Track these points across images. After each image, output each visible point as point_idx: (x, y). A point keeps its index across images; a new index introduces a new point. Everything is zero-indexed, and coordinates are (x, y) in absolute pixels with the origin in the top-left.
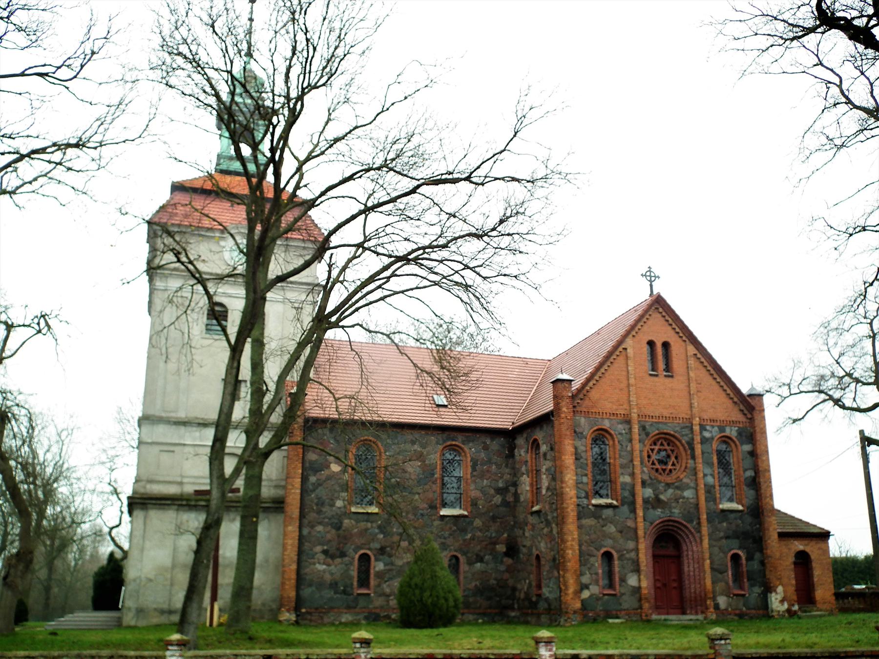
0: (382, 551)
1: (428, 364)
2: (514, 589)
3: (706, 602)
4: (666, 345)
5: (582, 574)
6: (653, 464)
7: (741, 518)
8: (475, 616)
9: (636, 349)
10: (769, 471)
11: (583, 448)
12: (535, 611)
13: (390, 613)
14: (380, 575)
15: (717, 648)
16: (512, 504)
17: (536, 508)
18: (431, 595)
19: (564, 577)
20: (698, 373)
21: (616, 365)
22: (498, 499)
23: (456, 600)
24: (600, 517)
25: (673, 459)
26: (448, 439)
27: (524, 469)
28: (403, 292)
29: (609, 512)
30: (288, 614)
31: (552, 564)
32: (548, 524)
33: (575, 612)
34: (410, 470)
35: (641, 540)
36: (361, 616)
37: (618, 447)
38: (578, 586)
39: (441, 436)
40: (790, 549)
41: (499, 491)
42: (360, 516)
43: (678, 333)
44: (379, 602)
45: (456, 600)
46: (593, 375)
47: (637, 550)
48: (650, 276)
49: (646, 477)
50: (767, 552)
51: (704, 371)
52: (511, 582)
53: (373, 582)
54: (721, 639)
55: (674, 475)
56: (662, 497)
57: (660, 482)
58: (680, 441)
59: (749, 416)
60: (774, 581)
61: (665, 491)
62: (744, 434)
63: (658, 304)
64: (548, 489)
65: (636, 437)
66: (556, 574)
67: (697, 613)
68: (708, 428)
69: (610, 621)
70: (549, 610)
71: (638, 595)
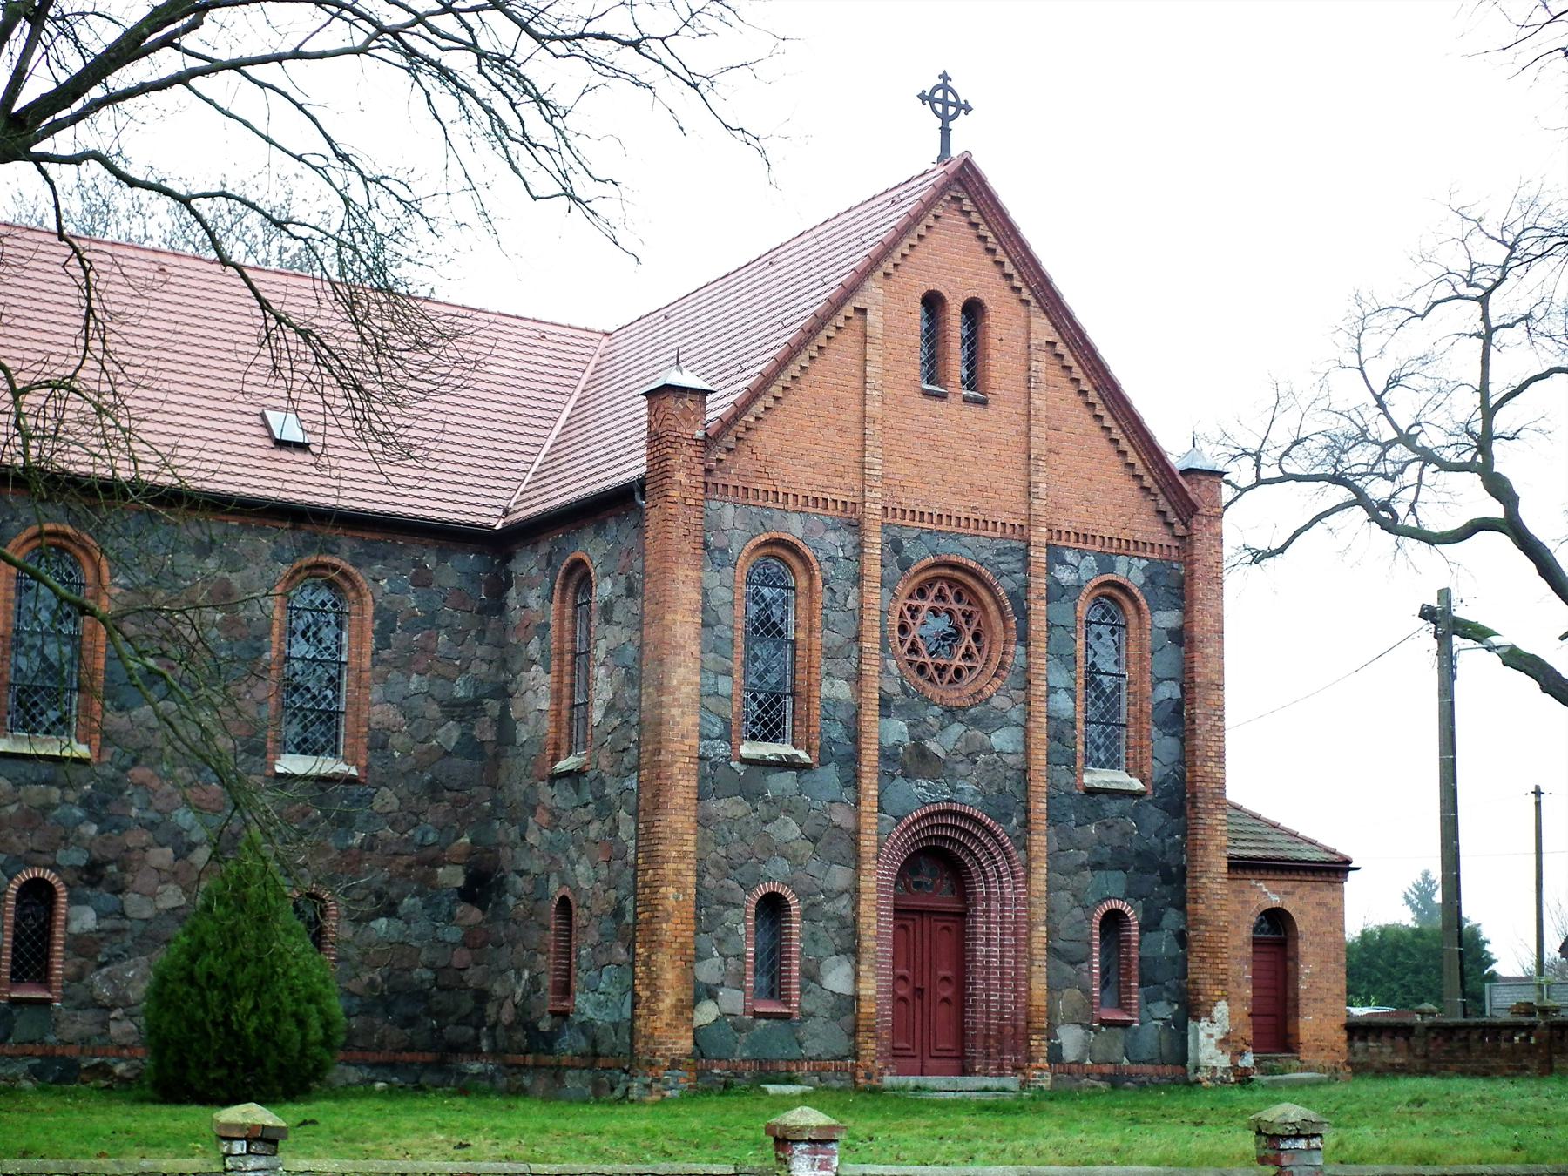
0: (92, 874)
1: (300, 300)
2: (482, 996)
3: (1028, 1040)
4: (973, 310)
5: (699, 957)
6: (913, 650)
7: (1136, 814)
8: (366, 1073)
9: (892, 315)
10: (1220, 687)
11: (725, 595)
12: (550, 1060)
13: (110, 1061)
14: (81, 945)
15: (1285, 1162)
16: (489, 750)
17: (562, 765)
18: (256, 1007)
19: (646, 964)
20: (1058, 399)
21: (831, 356)
22: (449, 734)
23: (327, 1025)
24: (761, 794)
25: (968, 639)
26: (309, 547)
27: (534, 648)
28: (236, 65)
29: (784, 782)
31: (609, 925)
32: (605, 808)
33: (675, 1064)
35: (869, 865)
36: (20, 1068)
37: (823, 597)
38: (688, 987)
39: (286, 535)
40: (1245, 903)
41: (459, 710)
42: (27, 767)
43: (1009, 277)
44: (79, 1025)
45: (327, 1025)
46: (767, 380)
47: (855, 892)
48: (945, 103)
49: (893, 688)
50: (1179, 912)
51: (1070, 392)
52: (473, 977)
53: (60, 966)
54: (1298, 1137)
55: (968, 683)
56: (932, 745)
57: (930, 703)
58: (991, 590)
59: (1180, 530)
60: (1208, 987)
61: (942, 728)
62: (1162, 580)
63: (964, 186)
64: (610, 709)
65: (874, 570)
66: (621, 953)
67: (1001, 1071)
68: (1070, 556)
69: (772, 1089)
70: (592, 1058)
71: (848, 1019)
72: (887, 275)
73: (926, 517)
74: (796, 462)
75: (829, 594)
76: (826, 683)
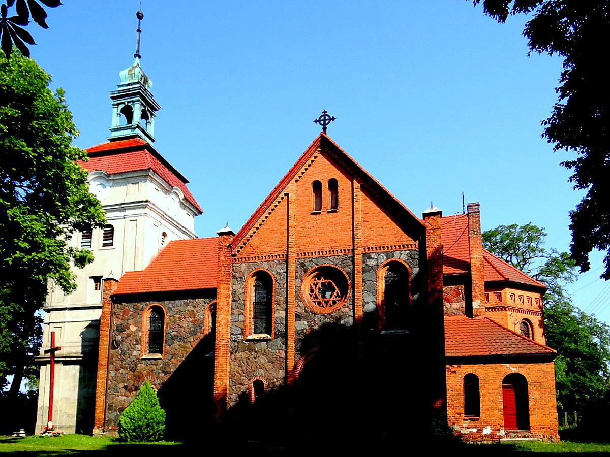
20: (363, 201)
30: (97, 430)
34: (185, 325)
40: (497, 372)
48: (325, 120)
72: (297, 181)
73: (313, 253)
74: (265, 246)
75: (278, 284)
76: (277, 313)
